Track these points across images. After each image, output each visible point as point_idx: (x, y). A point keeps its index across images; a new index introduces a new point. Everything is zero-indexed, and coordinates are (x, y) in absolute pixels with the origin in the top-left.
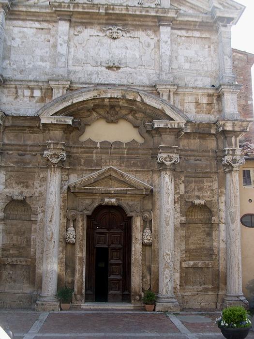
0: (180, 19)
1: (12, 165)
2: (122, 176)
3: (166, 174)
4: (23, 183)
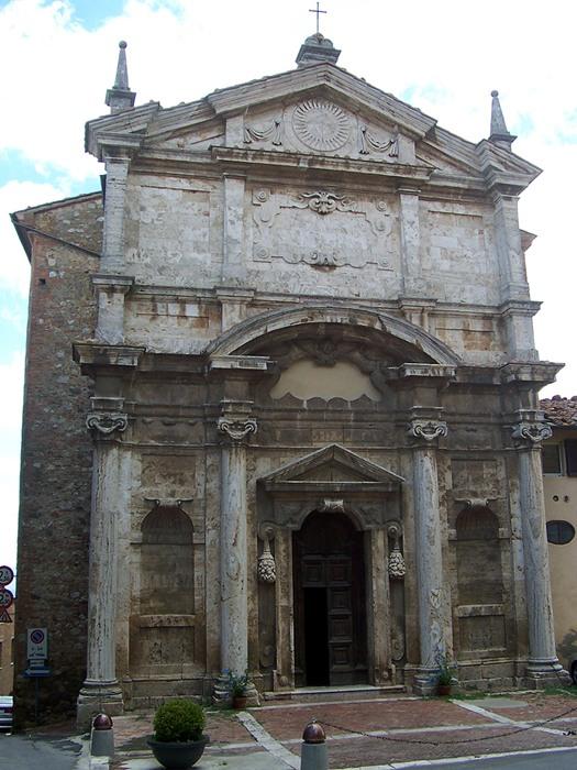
0: (432, 183)
1: (153, 442)
2: (353, 459)
4: (175, 475)
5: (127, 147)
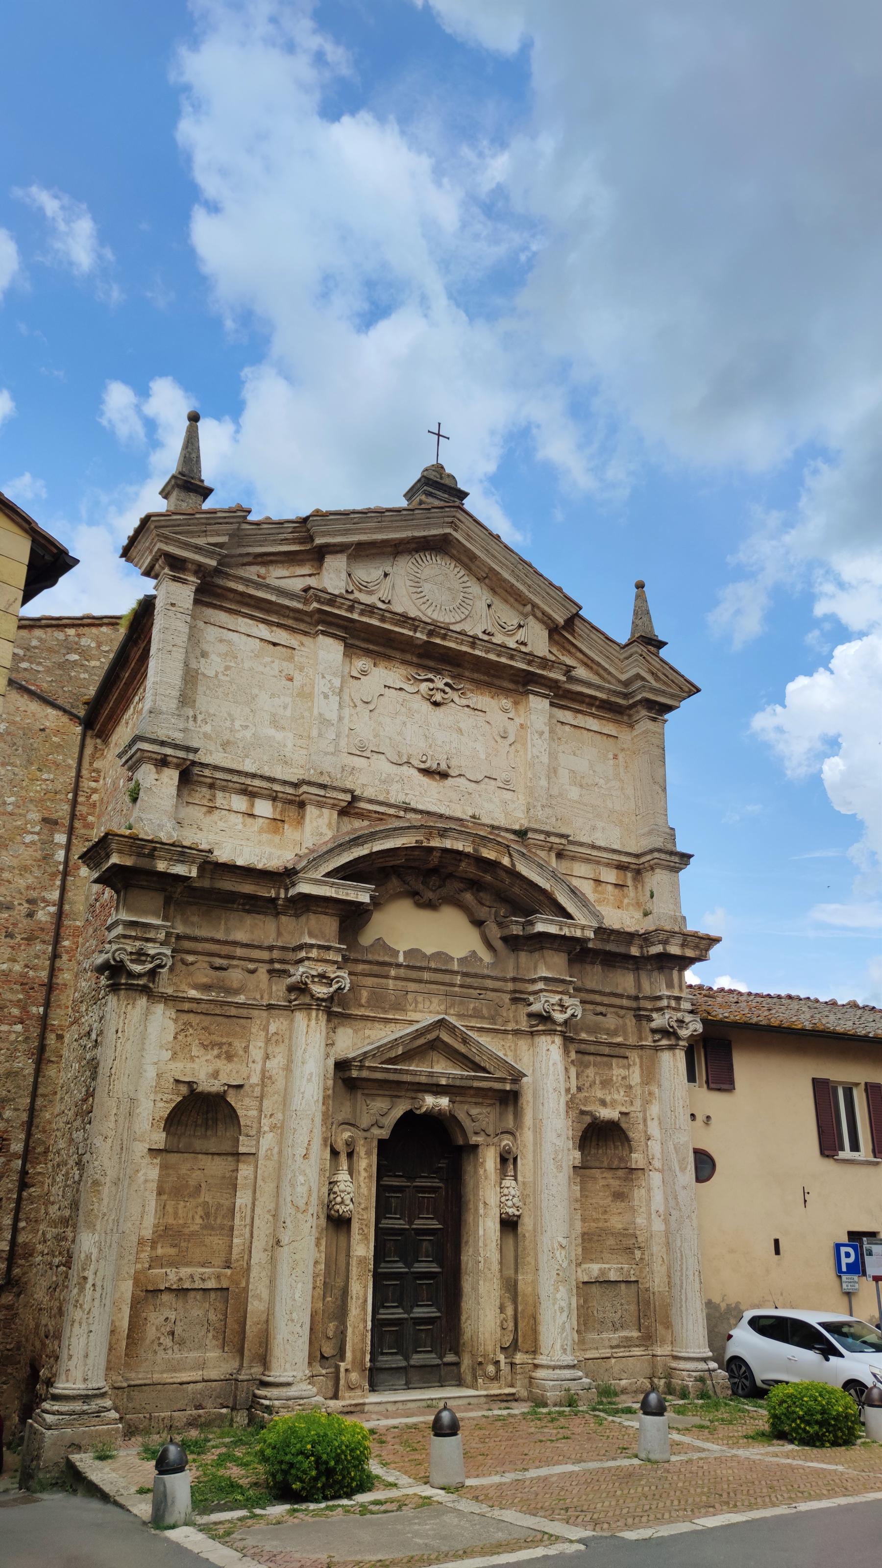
2: (465, 1041)
3: (553, 1042)
4: (220, 1045)
5: (193, 562)
